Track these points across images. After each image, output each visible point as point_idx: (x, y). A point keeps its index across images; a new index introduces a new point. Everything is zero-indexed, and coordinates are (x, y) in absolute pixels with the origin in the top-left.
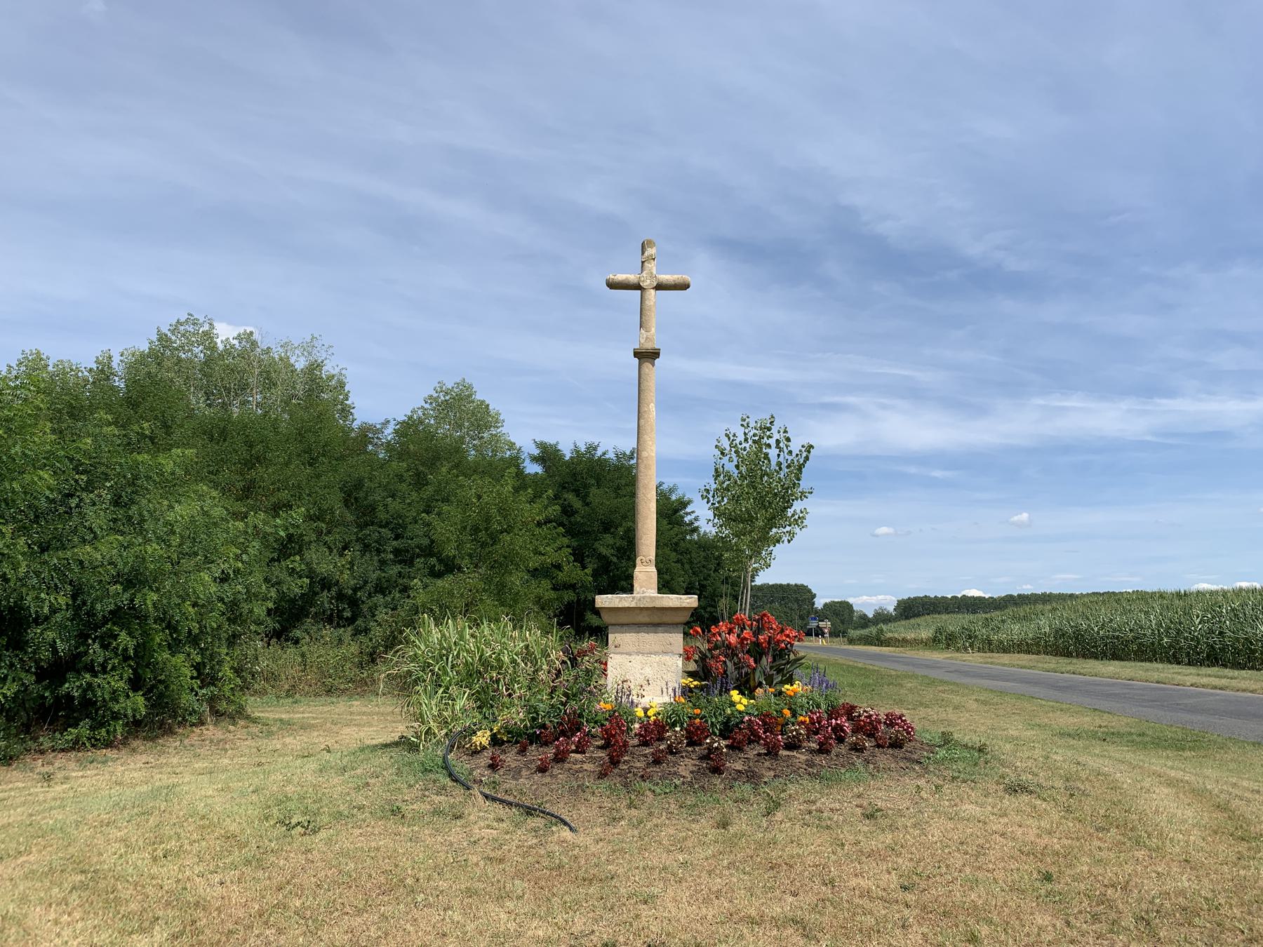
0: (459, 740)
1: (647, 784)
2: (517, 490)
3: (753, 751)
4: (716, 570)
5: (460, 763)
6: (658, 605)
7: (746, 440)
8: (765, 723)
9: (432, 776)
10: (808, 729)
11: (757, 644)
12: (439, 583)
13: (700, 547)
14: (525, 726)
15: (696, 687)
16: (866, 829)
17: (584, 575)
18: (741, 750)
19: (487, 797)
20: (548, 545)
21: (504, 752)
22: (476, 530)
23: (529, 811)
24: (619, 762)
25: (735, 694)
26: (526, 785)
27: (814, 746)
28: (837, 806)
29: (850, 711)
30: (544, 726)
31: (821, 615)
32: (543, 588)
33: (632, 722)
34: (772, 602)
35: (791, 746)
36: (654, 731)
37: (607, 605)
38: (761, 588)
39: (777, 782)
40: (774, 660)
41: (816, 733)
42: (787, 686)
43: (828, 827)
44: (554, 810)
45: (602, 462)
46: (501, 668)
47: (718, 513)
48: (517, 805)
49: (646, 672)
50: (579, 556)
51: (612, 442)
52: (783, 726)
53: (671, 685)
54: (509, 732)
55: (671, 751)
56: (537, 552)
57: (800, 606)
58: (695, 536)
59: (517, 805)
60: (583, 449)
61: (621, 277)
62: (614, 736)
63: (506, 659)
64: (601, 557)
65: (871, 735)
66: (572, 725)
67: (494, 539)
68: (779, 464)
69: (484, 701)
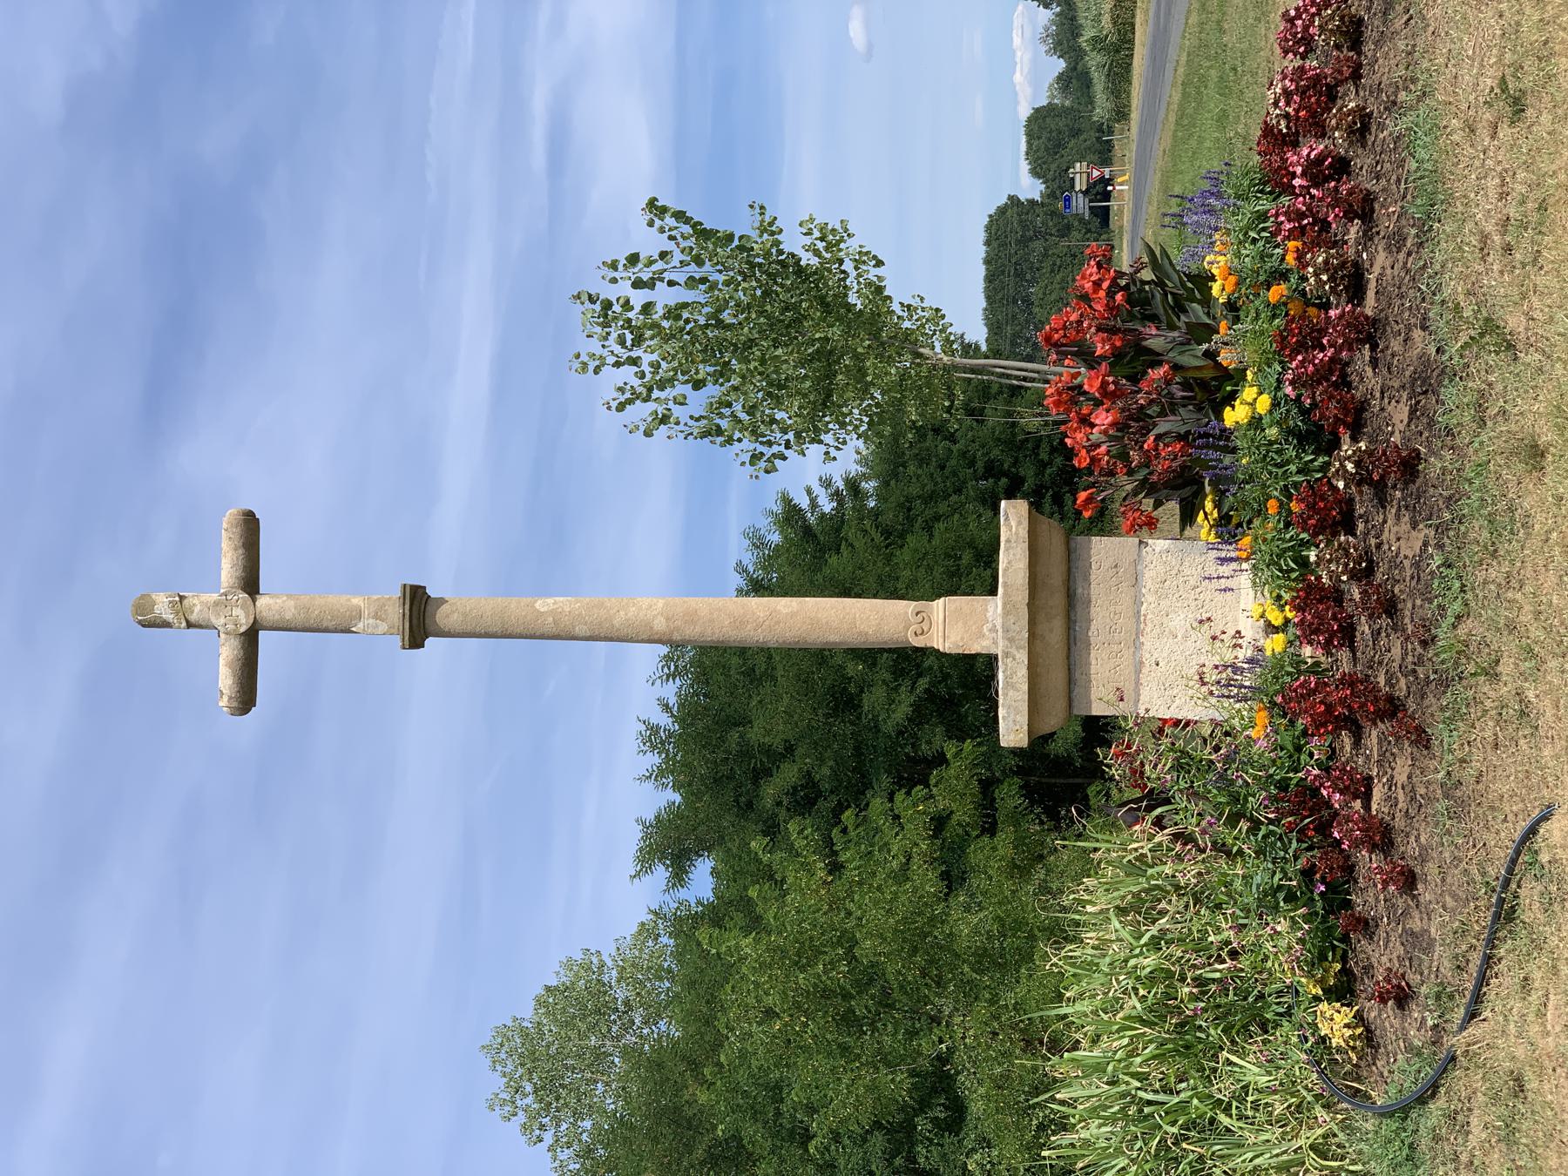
0: (1342, 1075)
1: (1443, 632)
2: (755, 923)
3: (1367, 379)
4: (952, 438)
5: (1395, 1077)
6: (1022, 596)
7: (634, 362)
8: (1301, 347)
9: (1424, 1143)
10: (1315, 244)
11: (1117, 356)
12: (976, 1107)
13: (895, 475)
14: (1307, 918)
15: (1218, 505)
16: (1546, 118)
17: (961, 755)
18: (1363, 406)
19: (1472, 1015)
20: (886, 847)
21: (1368, 969)
22: (848, 1021)
23: (1505, 914)
24: (1390, 699)
25: (1235, 416)
26: (1445, 919)
27: (1354, 230)
28: (1492, 183)
29: (1276, 140)
30: (1308, 874)
31: (1059, 185)
32: (990, 857)
33: (1298, 661)
34: (1028, 302)
35: (1355, 284)
36: (1319, 611)
37: (1023, 719)
38: (994, 327)
39: (1440, 325)
40: (1153, 318)
41: (1325, 226)
42: (1216, 289)
43: (1542, 207)
44: (1502, 855)
45: (687, 713)
46: (1169, 975)
47: (810, 432)
48: (1491, 943)
49: (1182, 627)
50: (915, 772)
51: (643, 692)
52: (1307, 303)
53: (1213, 569)
54: (1322, 957)
55: (1364, 574)
56: (903, 875)
57: (1037, 235)
58: (869, 486)
59: (1491, 943)
60: (654, 759)
61: (226, 680)
62: (1330, 708)
63: (1150, 962)
64: (919, 716)
65: (1332, 96)
66: (1304, 804)
67: (867, 977)
68: (692, 282)
69: (1250, 1016)
